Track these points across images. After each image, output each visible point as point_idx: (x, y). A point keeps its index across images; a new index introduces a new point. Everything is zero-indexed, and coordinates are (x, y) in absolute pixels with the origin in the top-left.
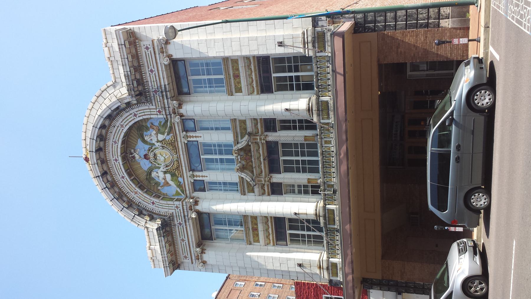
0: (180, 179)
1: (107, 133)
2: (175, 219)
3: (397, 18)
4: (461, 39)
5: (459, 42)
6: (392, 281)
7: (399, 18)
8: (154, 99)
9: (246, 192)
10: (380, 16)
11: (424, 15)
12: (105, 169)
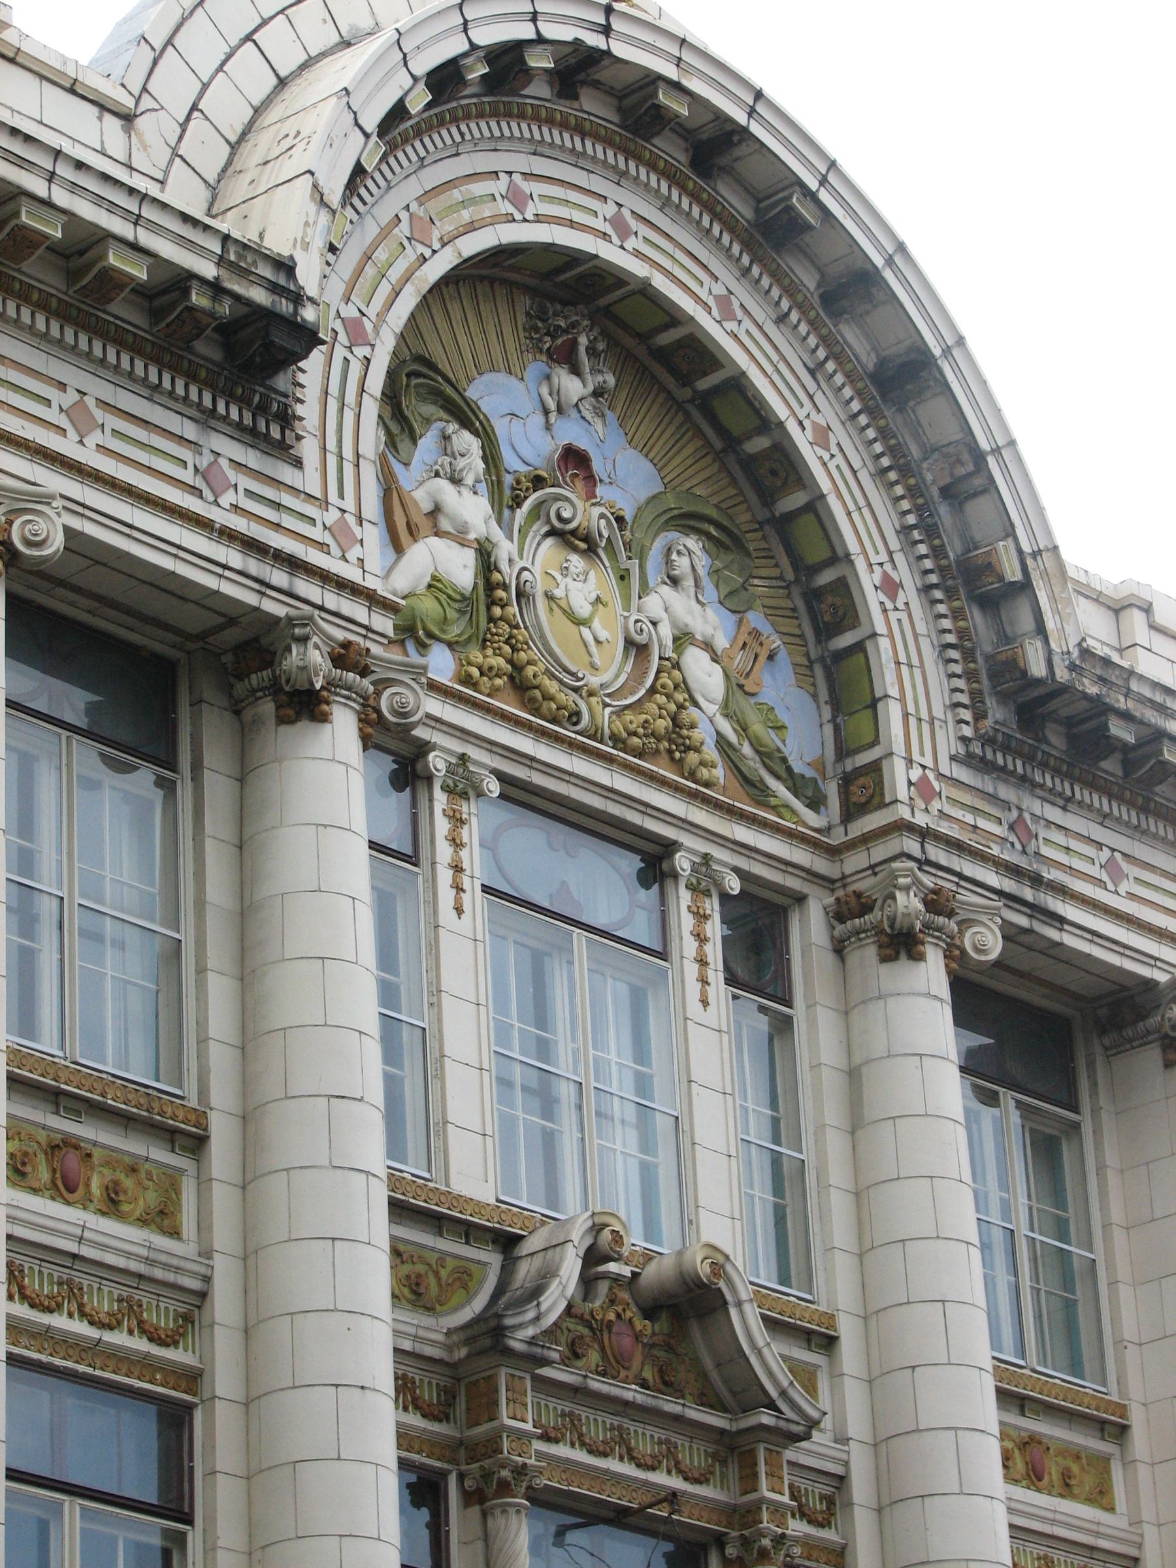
0: (441, 664)
1: (791, 290)
2: (252, 458)
12: (592, 105)
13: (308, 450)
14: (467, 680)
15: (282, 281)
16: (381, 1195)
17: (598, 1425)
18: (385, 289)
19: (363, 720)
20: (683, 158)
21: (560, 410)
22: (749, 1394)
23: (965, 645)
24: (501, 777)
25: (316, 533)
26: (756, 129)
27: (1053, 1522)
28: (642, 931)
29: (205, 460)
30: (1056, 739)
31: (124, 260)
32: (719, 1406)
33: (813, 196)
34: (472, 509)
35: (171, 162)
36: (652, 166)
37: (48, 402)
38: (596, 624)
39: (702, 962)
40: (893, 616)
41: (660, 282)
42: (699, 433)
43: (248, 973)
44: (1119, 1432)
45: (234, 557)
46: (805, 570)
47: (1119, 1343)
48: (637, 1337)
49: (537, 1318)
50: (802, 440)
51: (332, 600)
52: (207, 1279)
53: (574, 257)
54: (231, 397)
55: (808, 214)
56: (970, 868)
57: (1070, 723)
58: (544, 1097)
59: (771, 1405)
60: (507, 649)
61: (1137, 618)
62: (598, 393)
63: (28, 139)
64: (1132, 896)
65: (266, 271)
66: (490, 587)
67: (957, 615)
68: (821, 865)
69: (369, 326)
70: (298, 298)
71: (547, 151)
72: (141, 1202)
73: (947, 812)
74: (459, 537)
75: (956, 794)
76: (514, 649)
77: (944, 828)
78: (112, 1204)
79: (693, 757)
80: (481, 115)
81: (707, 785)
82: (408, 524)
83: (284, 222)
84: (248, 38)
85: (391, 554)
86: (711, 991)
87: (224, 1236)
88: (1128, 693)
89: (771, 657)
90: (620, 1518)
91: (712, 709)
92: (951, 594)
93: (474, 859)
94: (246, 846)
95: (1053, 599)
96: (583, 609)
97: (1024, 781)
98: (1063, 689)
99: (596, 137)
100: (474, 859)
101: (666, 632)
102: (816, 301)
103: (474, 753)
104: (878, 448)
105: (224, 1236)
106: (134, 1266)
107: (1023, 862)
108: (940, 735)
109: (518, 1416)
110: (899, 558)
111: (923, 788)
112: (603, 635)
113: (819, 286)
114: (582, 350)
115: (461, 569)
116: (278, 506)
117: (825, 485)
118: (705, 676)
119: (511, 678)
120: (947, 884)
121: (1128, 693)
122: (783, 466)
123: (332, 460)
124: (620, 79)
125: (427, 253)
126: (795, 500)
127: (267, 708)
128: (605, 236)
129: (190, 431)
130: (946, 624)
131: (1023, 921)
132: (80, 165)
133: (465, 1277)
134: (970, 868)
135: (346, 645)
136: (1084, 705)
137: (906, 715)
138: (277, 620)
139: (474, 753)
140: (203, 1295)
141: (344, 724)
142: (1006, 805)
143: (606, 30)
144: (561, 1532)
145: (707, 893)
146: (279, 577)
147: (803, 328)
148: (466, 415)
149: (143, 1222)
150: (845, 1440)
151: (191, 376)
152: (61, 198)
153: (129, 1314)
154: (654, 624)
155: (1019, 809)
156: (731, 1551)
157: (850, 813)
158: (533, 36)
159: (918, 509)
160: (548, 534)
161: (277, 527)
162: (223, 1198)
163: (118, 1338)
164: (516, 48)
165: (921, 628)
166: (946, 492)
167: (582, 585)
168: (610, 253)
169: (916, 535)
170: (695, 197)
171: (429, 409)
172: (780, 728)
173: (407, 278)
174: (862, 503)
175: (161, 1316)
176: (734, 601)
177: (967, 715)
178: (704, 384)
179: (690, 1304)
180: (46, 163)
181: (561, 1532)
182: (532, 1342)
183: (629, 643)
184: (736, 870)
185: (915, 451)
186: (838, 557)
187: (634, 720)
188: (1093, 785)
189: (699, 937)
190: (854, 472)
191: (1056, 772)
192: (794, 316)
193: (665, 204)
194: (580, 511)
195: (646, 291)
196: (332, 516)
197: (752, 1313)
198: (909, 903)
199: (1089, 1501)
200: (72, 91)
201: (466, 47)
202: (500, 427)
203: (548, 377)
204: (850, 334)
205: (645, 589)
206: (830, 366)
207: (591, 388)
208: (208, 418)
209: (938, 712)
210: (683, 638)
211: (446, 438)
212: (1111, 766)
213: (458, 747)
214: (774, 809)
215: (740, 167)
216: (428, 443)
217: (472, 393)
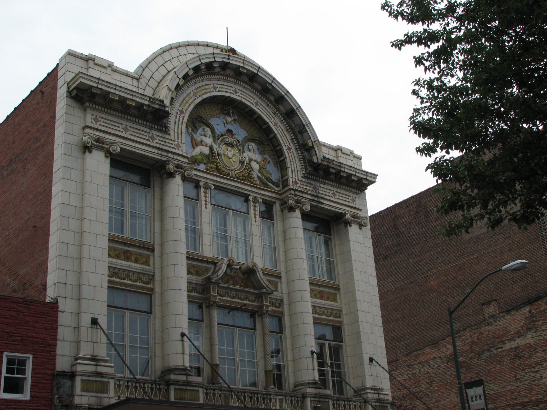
0: (202, 167)
1: (269, 100)
2: (160, 134)
9: (190, 262)
12: (229, 72)
13: (172, 132)
14: (207, 169)
16: (308, 283)
17: (232, 293)
18: (188, 105)
19: (182, 177)
21: (227, 123)
22: (262, 287)
23: (304, 158)
24: (214, 185)
25: (173, 146)
26: (259, 73)
28: (244, 209)
29: (151, 135)
30: (321, 172)
32: (257, 289)
33: (271, 84)
34: (209, 141)
36: (241, 81)
38: (233, 158)
39: (255, 214)
40: (290, 154)
41: (243, 100)
43: (162, 221)
44: (339, 289)
45: (156, 151)
46: (275, 147)
47: (338, 274)
48: (240, 278)
49: (217, 276)
50: (272, 126)
51: (175, 157)
52: (154, 273)
53: (227, 97)
54: (155, 124)
55: (270, 87)
56: (304, 195)
57: (324, 170)
58: (225, 238)
59: (265, 288)
61: (339, 152)
62: (234, 120)
63: (110, 83)
64: (337, 199)
65: (158, 102)
66: (212, 153)
67: (302, 153)
68: (278, 197)
69: (184, 111)
73: (301, 186)
74: (206, 145)
75: (302, 183)
77: (299, 189)
78: (136, 261)
79: (252, 180)
80: (207, 74)
81: (256, 184)
83: (164, 95)
84: (163, 65)
85: (192, 149)
86: (257, 219)
87: (157, 265)
88: (333, 164)
89: (269, 162)
90: (237, 309)
91: (256, 172)
92: (301, 149)
93: (208, 199)
94: (162, 200)
95: (318, 149)
96: (231, 156)
97: (315, 180)
98: (320, 164)
100: (208, 199)
101: (247, 159)
103: (209, 181)
104: (287, 126)
105: (157, 265)
106: (140, 271)
107: (315, 194)
108: (299, 174)
109: (214, 293)
110: (291, 144)
111: (296, 183)
112: (235, 160)
115: (206, 151)
116: (165, 142)
117: (276, 132)
118: (255, 166)
120: (300, 198)
121: (333, 164)
122: (269, 130)
123: (176, 134)
126: (272, 136)
127: (165, 176)
128: (232, 93)
129: (148, 130)
130: (300, 154)
131: (315, 204)
132: (121, 87)
133: (207, 270)
134: (304, 195)
135: (178, 164)
137: (292, 170)
138: (165, 161)
139: (209, 181)
140: (154, 276)
141: (178, 179)
142: (312, 185)
143: (229, 59)
144: (229, 312)
145: (256, 203)
146: (165, 154)
147: (272, 106)
148: (208, 125)
149: (142, 264)
150: (282, 293)
151: (147, 121)
152: (117, 92)
153: (139, 279)
156: (259, 313)
157: (283, 188)
159: (294, 136)
161: (165, 145)
162: (157, 260)
163: (137, 284)
164: (211, 63)
165: (295, 155)
166: (299, 132)
167: (230, 152)
168: (233, 96)
170: (250, 86)
172: (271, 174)
173: (192, 102)
175: (146, 279)
176: (262, 153)
177: (304, 170)
178: (255, 117)
179: (250, 272)
180: (114, 87)
181: (229, 312)
182: (216, 280)
183: (240, 161)
184: (262, 199)
185: (293, 126)
186: (280, 145)
187: (241, 174)
189: (255, 210)
191: (322, 178)
192: (270, 105)
193: (244, 87)
194: (229, 139)
195: (241, 102)
196: (176, 143)
197: (261, 273)
198: (291, 202)
199: (333, 301)
202: (215, 127)
204: (280, 107)
205: (244, 152)
206: (277, 113)
208: (151, 128)
209: (299, 169)
210: (251, 160)
211: (204, 129)
213: (205, 181)
214: (269, 188)
216: (200, 131)
217: (210, 121)
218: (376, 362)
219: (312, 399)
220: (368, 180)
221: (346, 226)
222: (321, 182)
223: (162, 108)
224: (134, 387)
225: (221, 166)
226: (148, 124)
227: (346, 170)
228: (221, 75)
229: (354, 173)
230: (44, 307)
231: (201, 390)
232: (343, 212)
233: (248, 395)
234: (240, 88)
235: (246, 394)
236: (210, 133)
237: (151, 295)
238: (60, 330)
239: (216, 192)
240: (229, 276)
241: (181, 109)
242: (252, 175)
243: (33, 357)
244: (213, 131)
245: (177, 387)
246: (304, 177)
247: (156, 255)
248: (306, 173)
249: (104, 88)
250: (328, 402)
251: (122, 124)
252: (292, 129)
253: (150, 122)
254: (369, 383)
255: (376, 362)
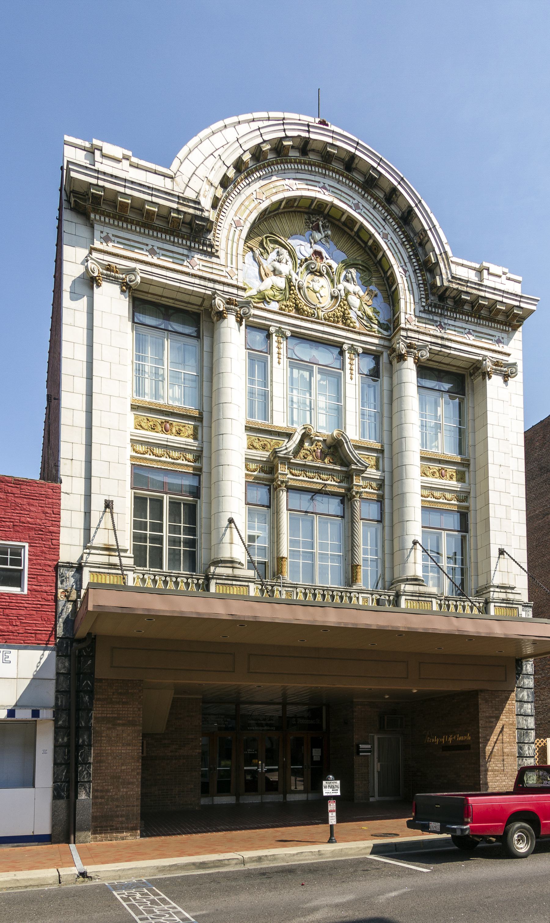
0: (274, 306)
1: (376, 199)
3: (525, 718)
4: (334, 814)
5: (331, 811)
6: (91, 699)
7: (526, 720)
8: (429, 319)
10: (528, 695)
11: (527, 752)
12: (312, 157)
15: (197, 206)
20: (342, 167)
27: (445, 486)
30: (450, 302)
31: (150, 206)
34: (286, 268)
35: (186, 188)
36: (333, 171)
37: (142, 249)
42: (358, 244)
54: (195, 242)
57: (454, 298)
60: (294, 300)
62: (326, 236)
66: (290, 287)
69: (242, 222)
70: (202, 210)
71: (301, 172)
72: (187, 433)
73: (414, 324)
76: (296, 300)
80: (277, 164)
82: (265, 274)
92: (421, 270)
93: (283, 351)
98: (447, 288)
99: (315, 165)
101: (342, 292)
102: (384, 200)
104: (402, 236)
113: (384, 196)
114: (320, 225)
115: (281, 283)
118: (354, 301)
119: (295, 308)
123: (229, 256)
124: (320, 147)
125: (261, 201)
131: (439, 349)
135: (229, 299)
136: (455, 292)
141: (231, 319)
142: (436, 322)
144: (312, 499)
154: (340, 291)
155: (440, 322)
158: (285, 136)
160: (309, 273)
169: (412, 257)
170: (347, 178)
171: (272, 246)
174: (397, 251)
176: (365, 284)
185: (412, 235)
188: (463, 313)
190: (396, 244)
191: (451, 311)
193: (339, 181)
200: (155, 173)
201: (262, 141)
203: (311, 235)
206: (388, 217)
207: (324, 235)
212: (467, 307)
215: (358, 166)
216: (273, 255)
218: (507, 553)
219: (408, 597)
220: (522, 308)
221: (484, 378)
222: (450, 318)
223: (198, 213)
224: (163, 581)
225: (302, 303)
226: (184, 242)
227: (488, 295)
228: (300, 163)
229: (500, 299)
230: (41, 487)
231: (434, 600)
232: (481, 358)
233: (460, 605)
234: (332, 183)
235: (335, 593)
236: (288, 257)
237: (199, 476)
238: (64, 515)
239: (295, 341)
240: (308, 450)
241: (236, 219)
242: (349, 314)
243: (30, 546)
244: (292, 254)
245: (218, 581)
246: (424, 311)
247: (204, 425)
248: (427, 305)
249: (108, 185)
250: (431, 601)
251: (147, 245)
252: (409, 240)
253: (187, 239)
254: (497, 580)
255: (507, 553)
